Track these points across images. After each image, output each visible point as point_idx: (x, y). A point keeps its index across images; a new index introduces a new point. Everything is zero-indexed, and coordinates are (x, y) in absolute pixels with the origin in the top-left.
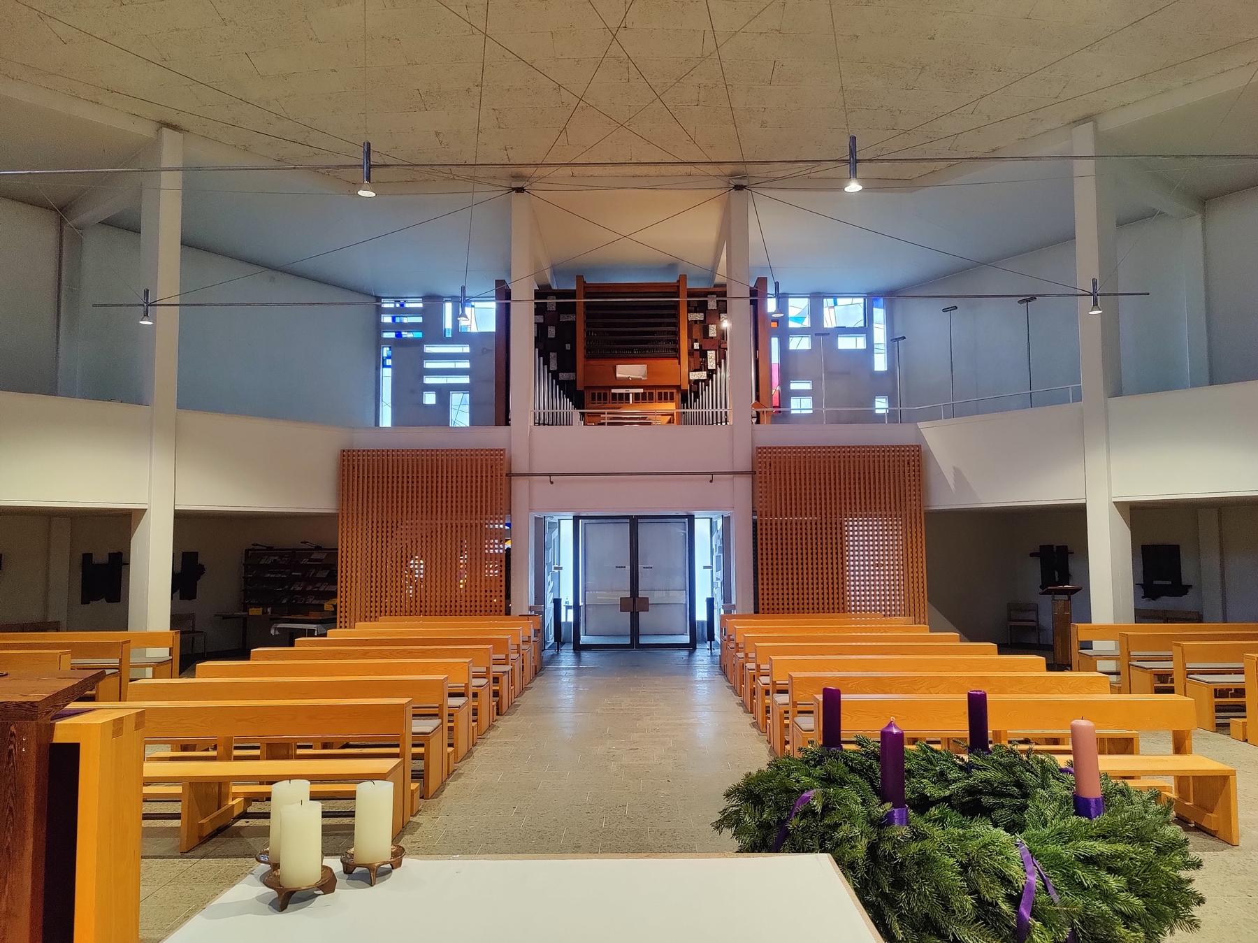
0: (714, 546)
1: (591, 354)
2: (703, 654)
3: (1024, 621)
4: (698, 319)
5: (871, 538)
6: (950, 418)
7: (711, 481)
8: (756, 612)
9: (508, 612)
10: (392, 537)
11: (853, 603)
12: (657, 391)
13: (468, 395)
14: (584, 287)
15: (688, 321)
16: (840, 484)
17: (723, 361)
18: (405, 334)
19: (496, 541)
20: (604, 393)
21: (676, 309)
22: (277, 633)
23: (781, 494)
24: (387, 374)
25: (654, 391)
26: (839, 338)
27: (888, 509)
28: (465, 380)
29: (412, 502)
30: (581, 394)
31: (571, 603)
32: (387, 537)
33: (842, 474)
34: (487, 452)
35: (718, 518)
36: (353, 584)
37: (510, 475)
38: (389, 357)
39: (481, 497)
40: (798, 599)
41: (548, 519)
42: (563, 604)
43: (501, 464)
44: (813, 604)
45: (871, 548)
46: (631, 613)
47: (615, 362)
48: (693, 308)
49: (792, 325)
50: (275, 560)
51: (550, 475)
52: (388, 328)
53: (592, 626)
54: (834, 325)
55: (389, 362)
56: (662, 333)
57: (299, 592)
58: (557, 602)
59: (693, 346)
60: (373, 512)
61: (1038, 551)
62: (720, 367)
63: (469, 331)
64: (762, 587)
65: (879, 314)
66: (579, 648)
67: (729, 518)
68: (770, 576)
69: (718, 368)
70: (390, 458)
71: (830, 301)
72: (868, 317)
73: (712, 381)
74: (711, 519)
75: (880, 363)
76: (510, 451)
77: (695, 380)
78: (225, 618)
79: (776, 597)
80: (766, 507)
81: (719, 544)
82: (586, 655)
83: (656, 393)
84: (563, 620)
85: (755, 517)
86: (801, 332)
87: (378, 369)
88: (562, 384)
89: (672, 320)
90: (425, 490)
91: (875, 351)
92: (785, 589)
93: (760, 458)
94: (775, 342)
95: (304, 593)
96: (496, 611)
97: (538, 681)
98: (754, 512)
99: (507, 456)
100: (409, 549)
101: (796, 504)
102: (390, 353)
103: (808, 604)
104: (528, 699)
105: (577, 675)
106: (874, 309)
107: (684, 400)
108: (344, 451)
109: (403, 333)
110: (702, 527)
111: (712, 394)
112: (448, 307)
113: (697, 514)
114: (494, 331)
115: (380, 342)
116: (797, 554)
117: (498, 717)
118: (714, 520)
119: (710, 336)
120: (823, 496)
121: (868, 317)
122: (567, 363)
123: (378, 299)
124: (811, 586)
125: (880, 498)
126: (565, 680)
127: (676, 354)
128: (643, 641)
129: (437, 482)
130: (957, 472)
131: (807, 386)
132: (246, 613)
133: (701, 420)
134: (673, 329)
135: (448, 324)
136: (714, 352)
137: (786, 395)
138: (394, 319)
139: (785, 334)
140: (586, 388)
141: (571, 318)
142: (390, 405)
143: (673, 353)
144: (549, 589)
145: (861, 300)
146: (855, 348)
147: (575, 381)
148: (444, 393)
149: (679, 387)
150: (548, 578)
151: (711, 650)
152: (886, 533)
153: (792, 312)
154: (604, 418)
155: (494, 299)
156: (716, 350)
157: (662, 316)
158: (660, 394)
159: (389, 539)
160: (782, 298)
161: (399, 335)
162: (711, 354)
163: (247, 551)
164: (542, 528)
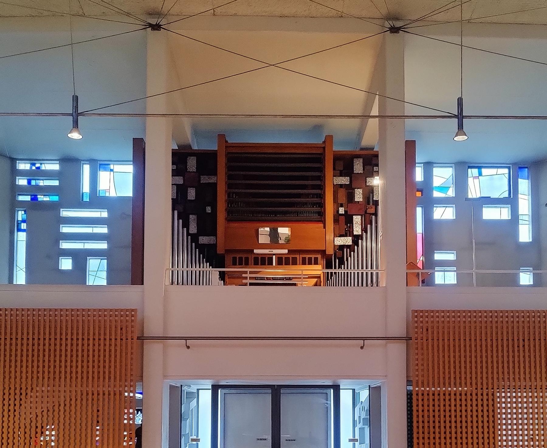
0: (357, 418)
4: (343, 183)
7: (362, 348)
10: (21, 405)
12: (302, 256)
13: (106, 261)
14: (226, 147)
15: (334, 184)
16: (470, 351)
17: (369, 226)
19: (131, 411)
21: (322, 171)
23: (444, 362)
24: (21, 238)
25: (298, 256)
27: (528, 379)
28: (103, 246)
37: (142, 338)
38: (23, 221)
39: (110, 361)
41: (185, 388)
43: (132, 327)
45: (509, 416)
47: (258, 225)
49: (436, 194)
51: (186, 339)
52: (23, 190)
55: (24, 226)
56: (307, 195)
59: (338, 211)
62: (366, 232)
63: (107, 195)
65: (524, 185)
67: (378, 388)
71: (475, 171)
72: (513, 187)
73: (358, 246)
74: (354, 390)
81: (364, 415)
83: (299, 257)
85: (411, 388)
86: (445, 202)
87: (12, 233)
88: (202, 248)
89: (318, 182)
90: (47, 354)
91: (520, 222)
94: (419, 211)
98: (409, 382)
99: (139, 317)
100: (39, 418)
101: (487, 373)
102: (25, 216)
107: (329, 265)
109: (38, 196)
110: (346, 397)
112: (86, 169)
113: (343, 384)
115: (14, 205)
118: (356, 391)
120: (484, 365)
121: (513, 187)
123: (13, 161)
125: (503, 367)
127: (321, 217)
131: (451, 256)
133: (346, 281)
134: (318, 191)
135: (86, 188)
136: (360, 217)
138: (29, 182)
140: (228, 251)
141: (212, 180)
142: (24, 270)
143: (316, 216)
146: (499, 218)
147: (214, 246)
153: (437, 182)
154: (246, 278)
155: (132, 163)
156: (362, 215)
157: (306, 178)
158: (304, 259)
159: (17, 408)
160: (428, 166)
161: (34, 198)
162: (357, 219)
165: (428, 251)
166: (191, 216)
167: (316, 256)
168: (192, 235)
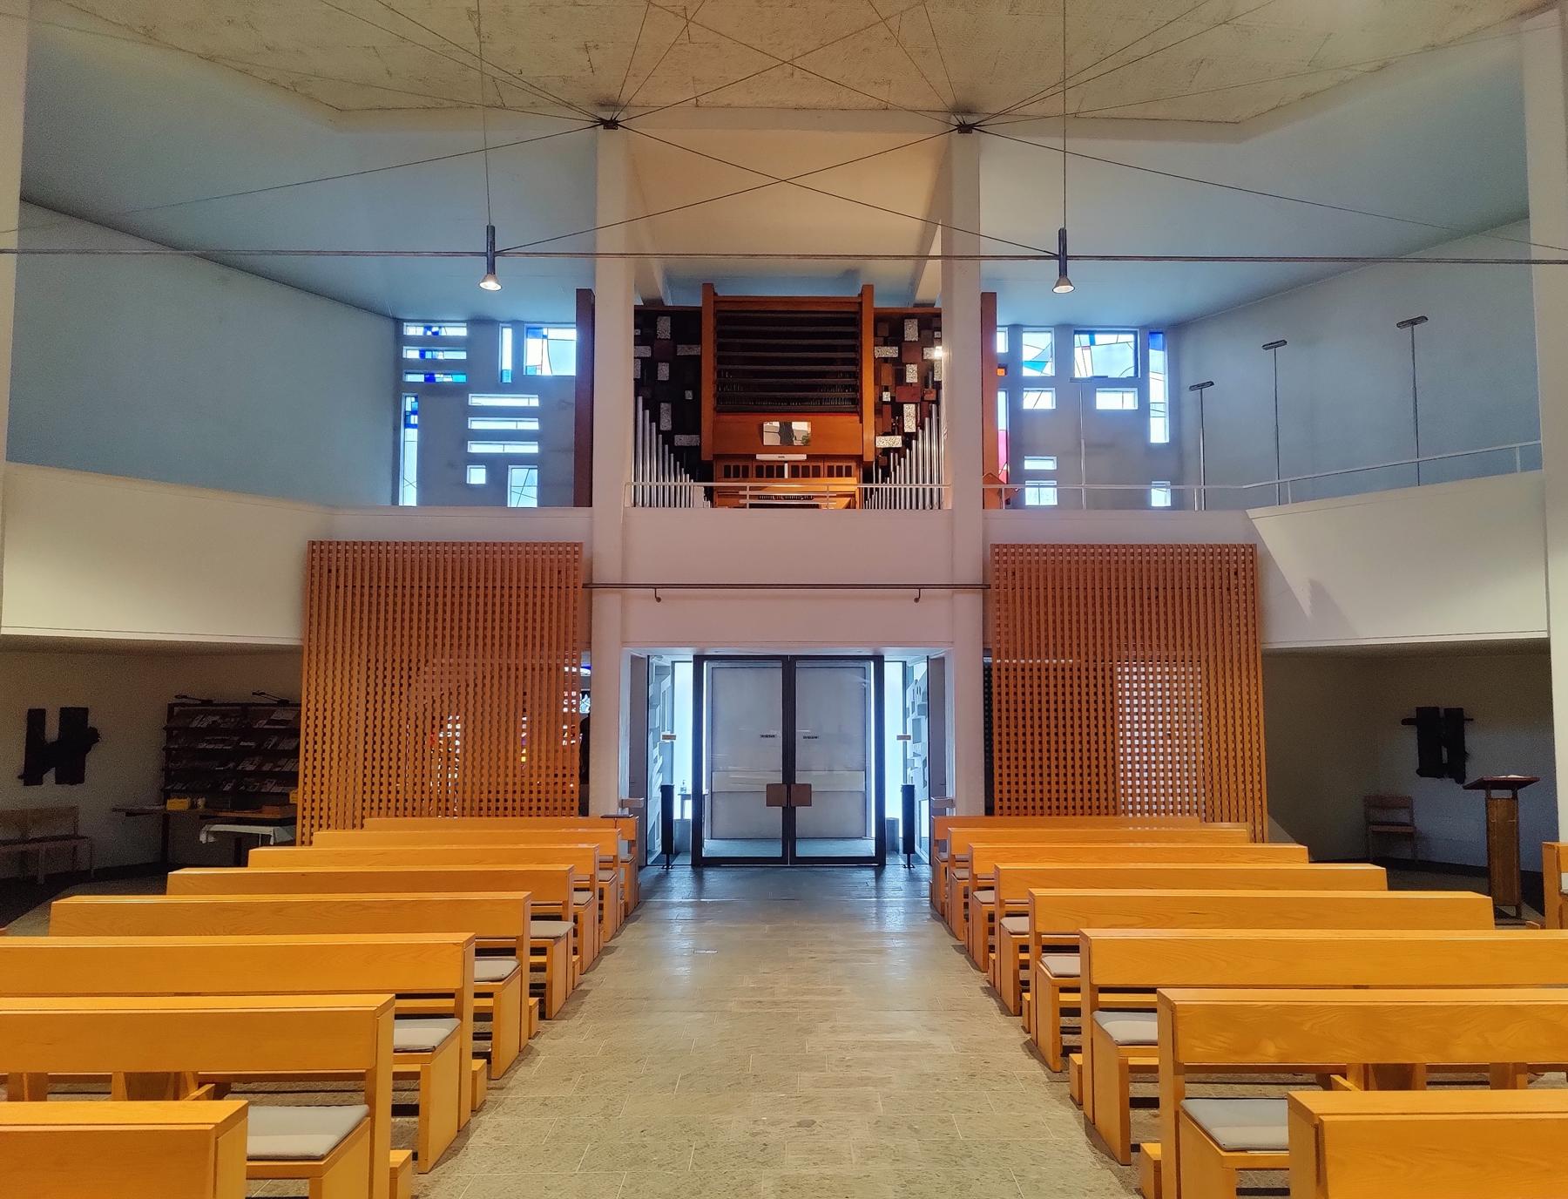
0: (909, 704)
1: (725, 404)
2: (896, 870)
3: (1393, 824)
4: (889, 355)
5: (1135, 694)
6: (1275, 505)
7: (917, 600)
8: (989, 810)
9: (584, 810)
11: (1130, 791)
12: (827, 464)
13: (536, 471)
14: (715, 302)
17: (927, 419)
18: (439, 378)
19: (574, 694)
20: (846, 467)
21: (857, 338)
22: (211, 839)
24: (411, 437)
25: (821, 464)
26: (1098, 394)
28: (532, 448)
29: (411, 628)
30: (710, 465)
31: (689, 791)
32: (401, 685)
33: (1113, 590)
34: (552, 549)
35: (918, 661)
36: (334, 764)
37: (589, 586)
38: (414, 412)
40: (1058, 791)
41: (654, 660)
42: (677, 791)
44: (1041, 783)
46: (783, 808)
47: (763, 417)
48: (882, 339)
49: (1027, 372)
50: (214, 722)
51: (655, 587)
52: (412, 367)
53: (720, 828)
54: (1090, 374)
55: (414, 419)
56: (835, 374)
57: (249, 774)
58: (667, 791)
59: (881, 398)
60: (361, 643)
61: (1414, 715)
62: (923, 428)
63: (538, 373)
64: (1000, 771)
65: (1158, 359)
66: (701, 864)
68: (1013, 754)
69: (920, 431)
70: (383, 556)
71: (1085, 338)
72: (1142, 362)
73: (911, 450)
75: (1159, 432)
76: (591, 548)
77: (884, 449)
78: (129, 814)
79: (1022, 787)
80: (1007, 642)
81: (919, 700)
82: (712, 877)
83: (823, 466)
84: (677, 816)
85: (989, 660)
86: (1040, 384)
87: (396, 430)
91: (1152, 413)
92: (1037, 775)
93: (998, 562)
94: (1002, 397)
95: (259, 775)
96: (564, 808)
97: (631, 933)
98: (987, 651)
100: (437, 705)
102: (416, 405)
103: (1058, 799)
104: (610, 977)
105: (698, 920)
106: (1150, 350)
108: (314, 543)
109: (436, 376)
110: (893, 673)
111: (911, 471)
112: (507, 335)
114: (573, 373)
115: (400, 389)
116: (1056, 718)
117: (543, 1023)
118: (909, 665)
119: (908, 381)
121: (1142, 362)
122: (687, 419)
123: (398, 323)
124: (1078, 771)
126: (678, 929)
127: (856, 407)
128: (803, 850)
129: (469, 596)
130: (1317, 591)
131: (1049, 465)
132: (162, 807)
133: (893, 502)
134: (852, 368)
135: (507, 363)
137: (1018, 476)
138: (422, 354)
139: (1016, 386)
140: (718, 457)
142: (415, 484)
143: (848, 405)
144: (654, 769)
145: (1131, 338)
146: (1121, 408)
147: (698, 449)
148: (498, 467)
149: (861, 457)
150: (654, 752)
151: (909, 867)
152: (1167, 685)
153: (1028, 354)
154: (744, 497)
155: (575, 326)
156: (916, 404)
161: (430, 378)
162: (909, 410)
163: (171, 707)
164: (642, 672)
165: (1015, 457)
166: (663, 405)
167: (849, 464)
168: (663, 433)
